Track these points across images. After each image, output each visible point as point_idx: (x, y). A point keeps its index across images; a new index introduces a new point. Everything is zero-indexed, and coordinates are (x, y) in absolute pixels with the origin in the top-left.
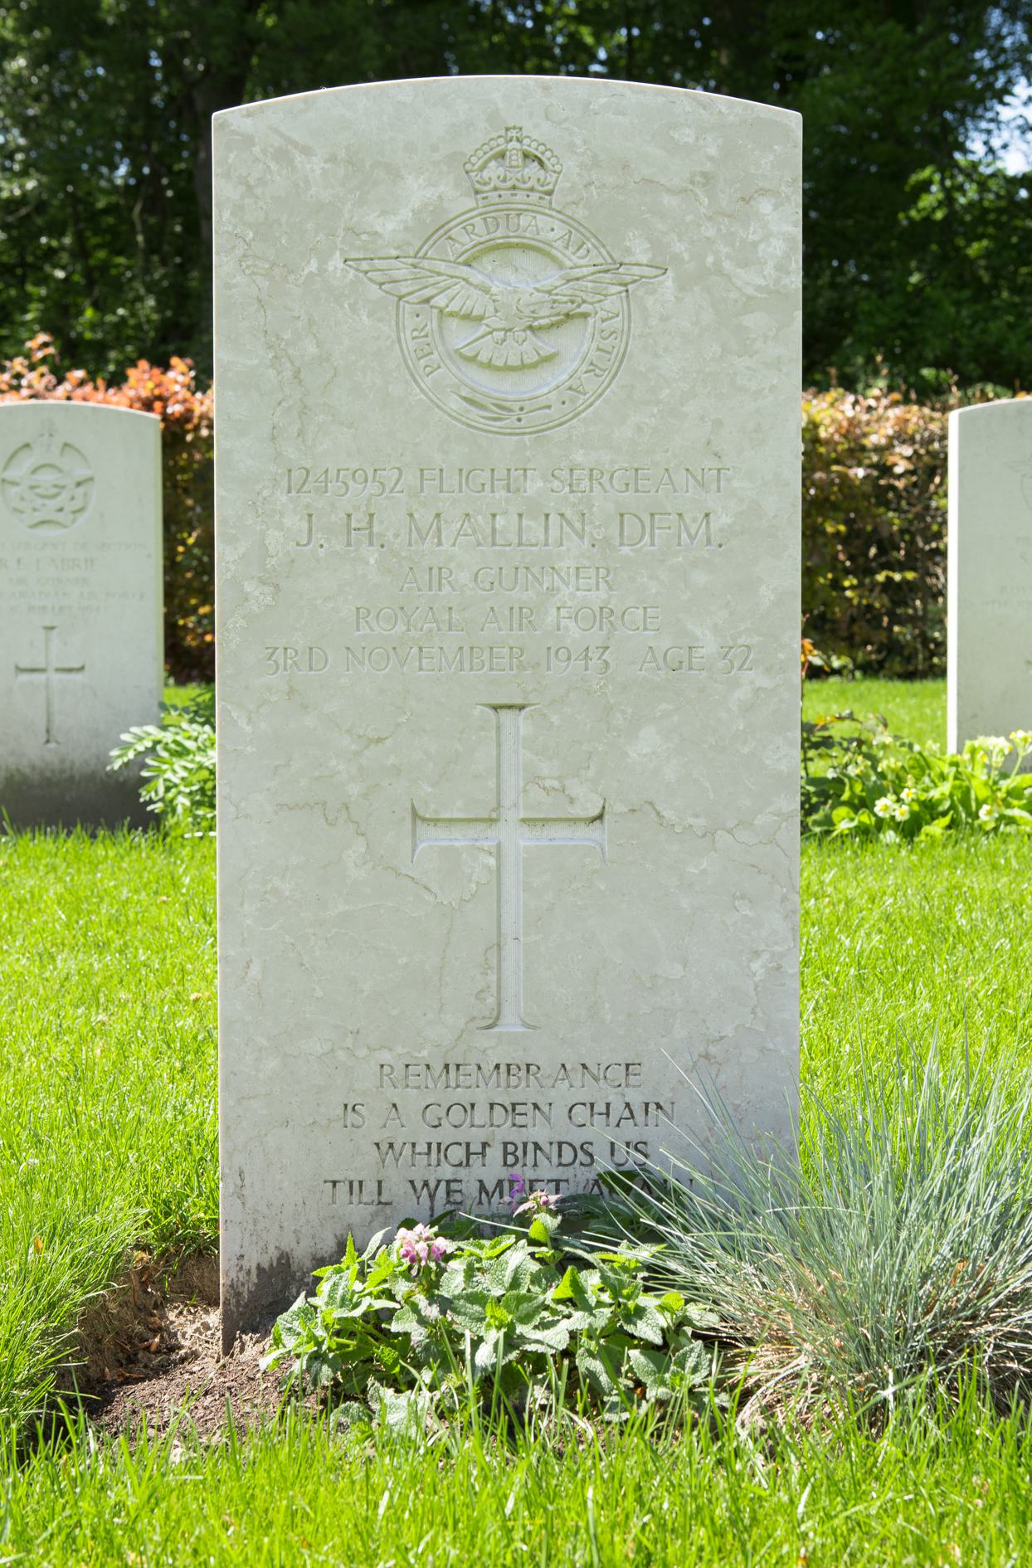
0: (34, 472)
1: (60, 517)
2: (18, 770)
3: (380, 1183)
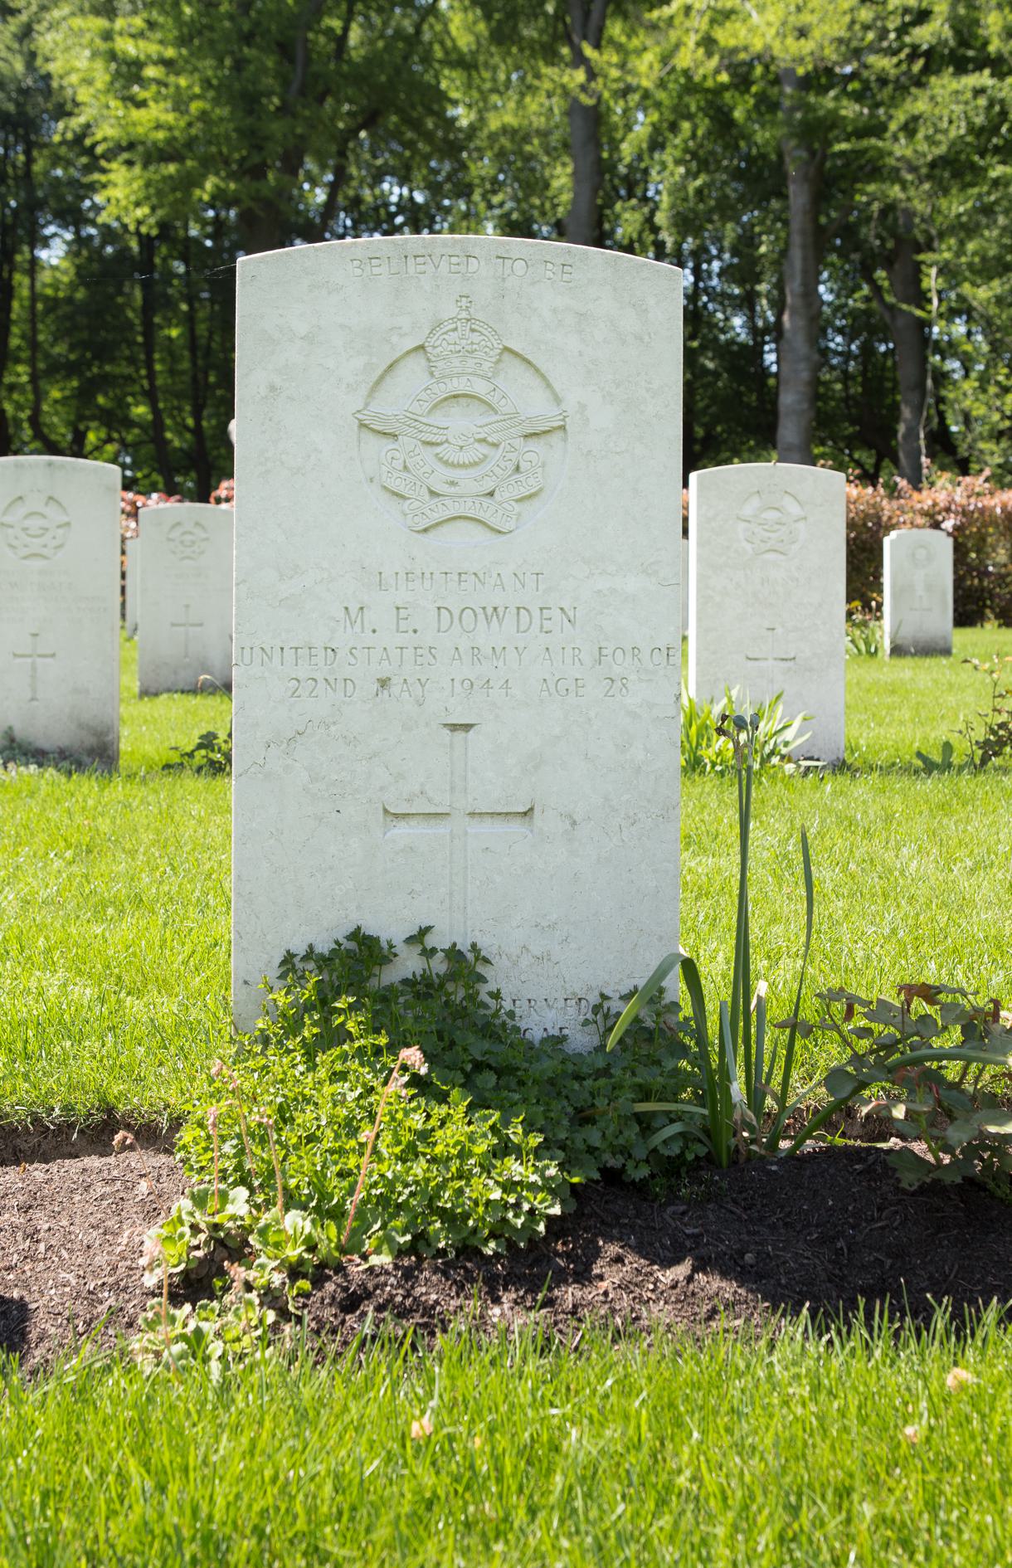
1: (45, 552)
2: (80, 726)
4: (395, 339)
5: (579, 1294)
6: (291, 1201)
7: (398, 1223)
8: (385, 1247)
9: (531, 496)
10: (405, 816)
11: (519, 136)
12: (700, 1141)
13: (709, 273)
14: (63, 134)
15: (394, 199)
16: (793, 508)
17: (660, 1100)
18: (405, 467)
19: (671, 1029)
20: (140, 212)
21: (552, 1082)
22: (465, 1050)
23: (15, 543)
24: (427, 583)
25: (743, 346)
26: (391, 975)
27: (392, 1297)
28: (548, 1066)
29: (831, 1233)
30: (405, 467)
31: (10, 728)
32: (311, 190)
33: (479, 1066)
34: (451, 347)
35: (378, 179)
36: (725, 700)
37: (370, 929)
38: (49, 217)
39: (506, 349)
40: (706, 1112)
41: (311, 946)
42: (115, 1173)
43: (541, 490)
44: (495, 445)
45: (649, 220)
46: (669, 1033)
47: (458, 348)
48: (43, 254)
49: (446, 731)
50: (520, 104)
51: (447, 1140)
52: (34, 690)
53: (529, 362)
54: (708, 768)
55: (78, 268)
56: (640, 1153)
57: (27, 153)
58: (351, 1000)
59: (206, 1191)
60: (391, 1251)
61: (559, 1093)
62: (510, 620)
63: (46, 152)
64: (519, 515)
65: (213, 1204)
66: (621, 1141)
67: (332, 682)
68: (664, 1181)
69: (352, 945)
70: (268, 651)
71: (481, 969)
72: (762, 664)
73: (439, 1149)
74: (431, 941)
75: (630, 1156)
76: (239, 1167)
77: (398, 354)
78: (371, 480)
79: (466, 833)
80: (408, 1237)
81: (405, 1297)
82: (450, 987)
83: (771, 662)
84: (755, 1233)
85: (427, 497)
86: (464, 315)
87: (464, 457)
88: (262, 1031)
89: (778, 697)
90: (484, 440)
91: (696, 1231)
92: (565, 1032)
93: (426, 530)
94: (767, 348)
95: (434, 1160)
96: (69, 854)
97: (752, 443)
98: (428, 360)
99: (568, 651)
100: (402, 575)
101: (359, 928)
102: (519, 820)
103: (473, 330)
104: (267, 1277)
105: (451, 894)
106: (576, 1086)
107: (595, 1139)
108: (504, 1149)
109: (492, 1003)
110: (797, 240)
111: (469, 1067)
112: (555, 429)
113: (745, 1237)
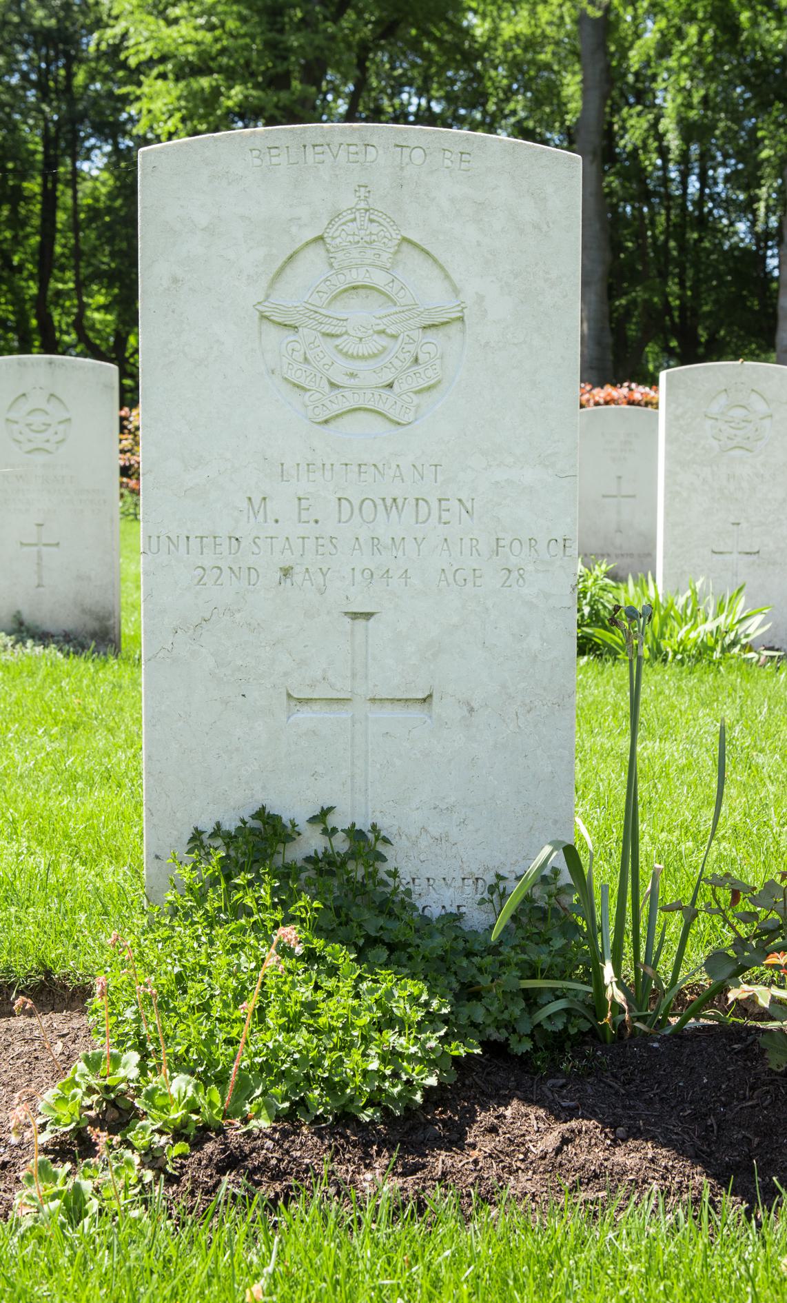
0: (29, 413)
1: (47, 446)
2: (84, 611)
3: (634, 496)
4: (294, 230)
5: (449, 1162)
6: (180, 1064)
7: (279, 1090)
8: (264, 1112)
9: (429, 388)
10: (308, 701)
11: (532, 44)
12: (585, 1018)
13: (714, 179)
14: (98, 45)
15: (412, 109)
16: (760, 406)
17: (547, 978)
18: (306, 359)
19: (565, 909)
21: (442, 959)
22: (360, 926)
23: (20, 438)
24: (328, 474)
25: (746, 251)
26: (295, 853)
27: (267, 1160)
28: (438, 943)
29: (703, 1110)
30: (306, 359)
31: (19, 612)
32: (335, 101)
33: (372, 942)
34: (350, 238)
35: (397, 92)
36: (689, 593)
37: (273, 810)
38: (89, 130)
39: (405, 240)
40: (591, 989)
41: (218, 824)
42: (36, 1033)
43: (439, 382)
44: (395, 337)
45: (655, 125)
46: (562, 913)
47: (357, 239)
48: (85, 166)
49: (347, 620)
50: (533, 13)
51: (332, 1011)
52: (40, 577)
53: (428, 253)
54: (670, 658)
56: (525, 1028)
57: (68, 67)
58: (249, 876)
59: (100, 1055)
60: (270, 1116)
61: (448, 969)
62: (409, 508)
63: (84, 67)
64: (418, 406)
65: (105, 1067)
66: (506, 1016)
67: (236, 571)
68: (546, 1054)
69: (257, 824)
70: (175, 540)
71: (381, 848)
72: (727, 557)
73: (322, 1021)
74: (333, 821)
75: (514, 1031)
76: (138, 1034)
77: (297, 246)
78: (273, 372)
79: (367, 718)
80: (287, 1104)
81: (280, 1160)
82: (351, 865)
83: (735, 556)
84: (631, 1107)
85: (327, 388)
86: (363, 205)
87: (363, 349)
88: (171, 903)
89: (740, 590)
90: (383, 332)
91: (572, 1103)
92: (463, 909)
93: (326, 422)
94: (769, 253)
95: (317, 1031)
96: (55, 730)
97: (754, 346)
98: (328, 251)
99: (466, 541)
100: (303, 467)
101: (264, 808)
102: (418, 706)
103: (371, 221)
104: (148, 1139)
105: (353, 777)
106: (465, 963)
107: (480, 1015)
108: (389, 1021)
109: (390, 880)
111: (361, 942)
112: (453, 320)
113: (619, 1111)
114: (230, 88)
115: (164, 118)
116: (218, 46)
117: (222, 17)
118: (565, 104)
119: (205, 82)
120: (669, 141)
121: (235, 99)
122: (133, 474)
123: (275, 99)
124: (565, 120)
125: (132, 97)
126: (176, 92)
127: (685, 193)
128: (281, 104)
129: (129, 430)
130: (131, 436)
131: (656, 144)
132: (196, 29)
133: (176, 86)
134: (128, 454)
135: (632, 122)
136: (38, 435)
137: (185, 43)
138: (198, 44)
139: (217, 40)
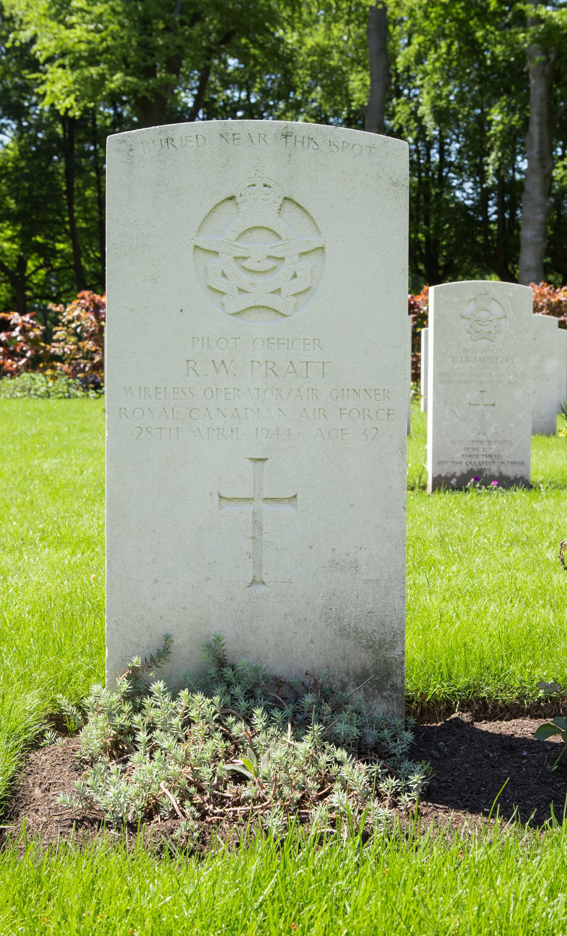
1: (275, 302)
2: (343, 632)
11: (323, 52)
14: (13, 42)
20: (70, 101)
23: (221, 284)
31: (218, 639)
49: (250, 463)
52: (258, 566)
55: (21, 147)
94: (490, 203)
110: (535, 119)
114: (112, 75)
115: (63, 97)
116: (104, 44)
117: (107, 24)
118: (351, 95)
119: (93, 71)
120: (426, 122)
121: (117, 83)
122: (66, 360)
123: (146, 84)
124: (351, 106)
125: (39, 81)
126: (71, 79)
127: (428, 161)
128: (150, 88)
129: (63, 323)
130: (65, 328)
131: (416, 124)
132: (89, 31)
133: (72, 73)
134: (62, 343)
135: (398, 109)
136: (257, 279)
137: (80, 42)
138: (89, 42)
139: (103, 40)
